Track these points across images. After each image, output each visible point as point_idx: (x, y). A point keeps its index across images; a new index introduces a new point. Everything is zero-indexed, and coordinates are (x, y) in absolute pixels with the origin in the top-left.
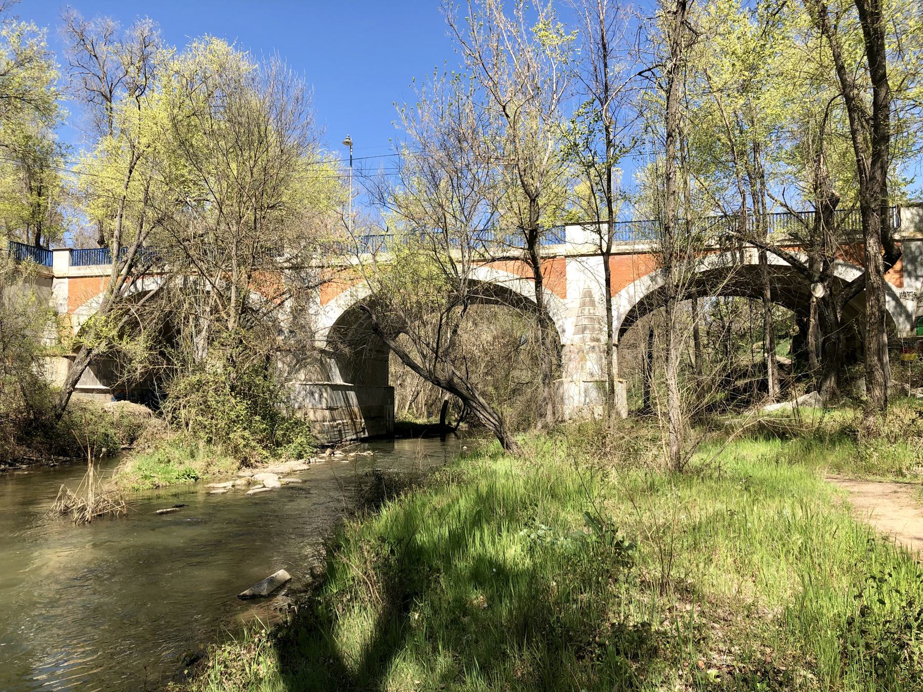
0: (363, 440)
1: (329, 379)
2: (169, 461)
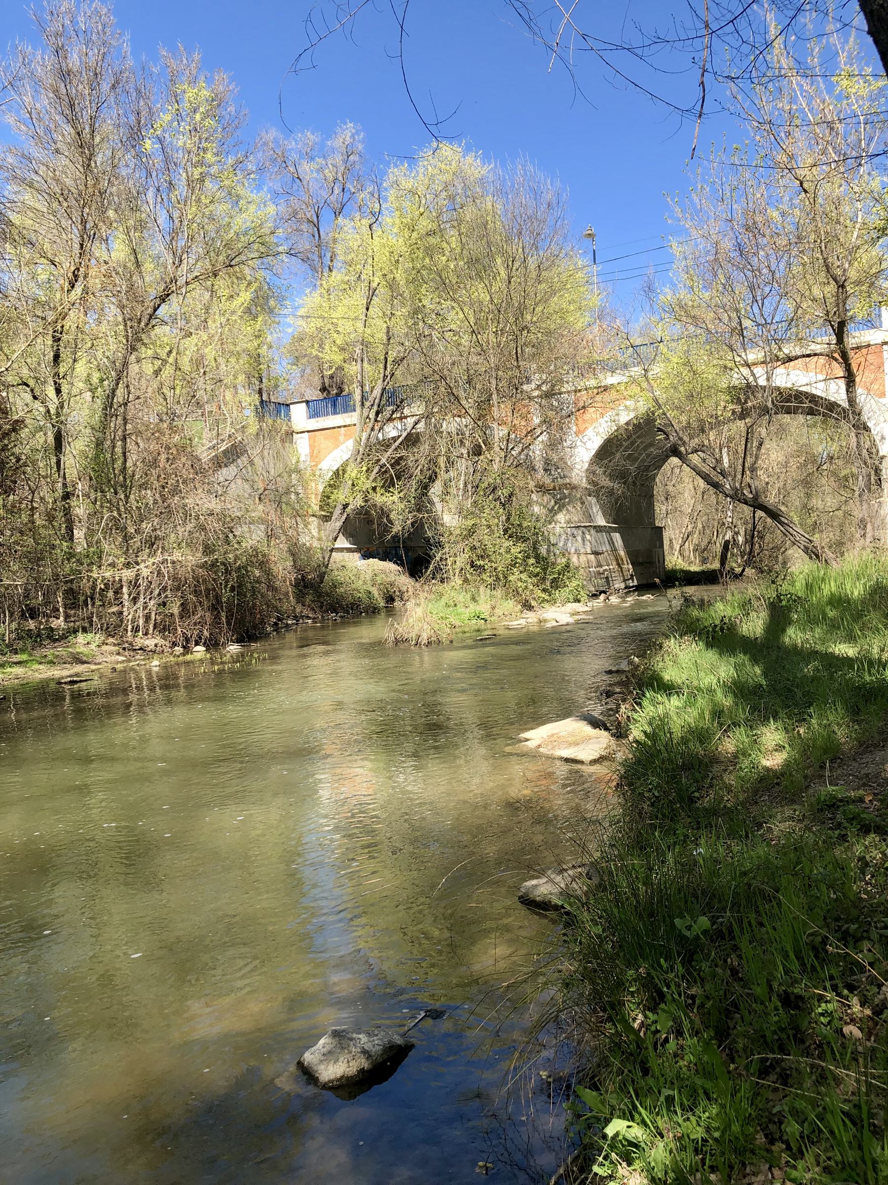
2: (455, 605)
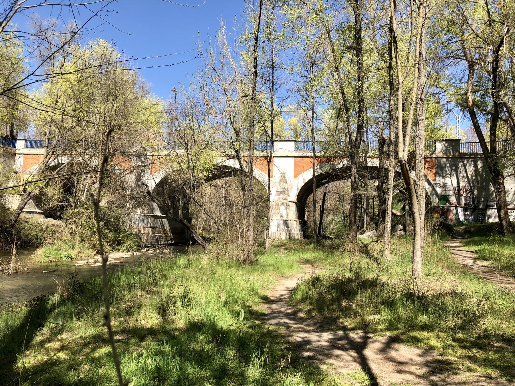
0: (171, 245)
1: (153, 213)
2: (60, 250)
